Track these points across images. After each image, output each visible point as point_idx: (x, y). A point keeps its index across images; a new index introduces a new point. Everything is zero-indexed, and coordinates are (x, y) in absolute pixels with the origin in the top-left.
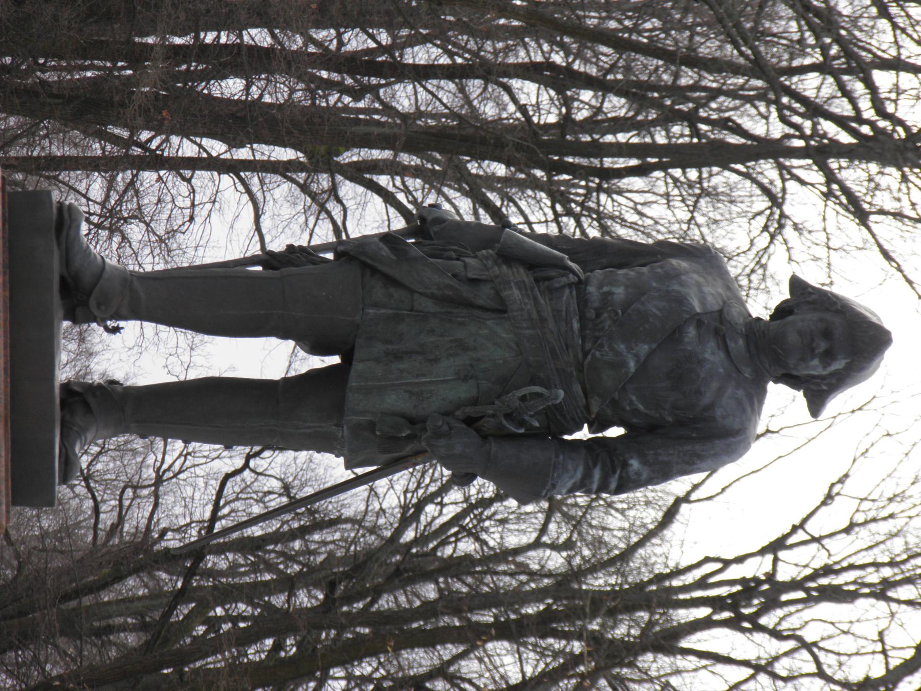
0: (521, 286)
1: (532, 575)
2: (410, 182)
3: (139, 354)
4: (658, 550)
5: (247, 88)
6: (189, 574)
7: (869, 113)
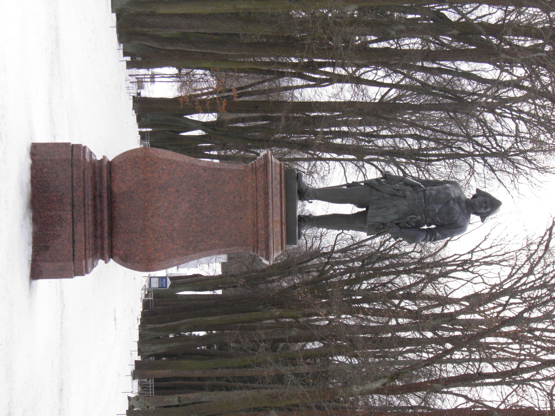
0: (410, 191)
1: (413, 259)
2: (382, 163)
3: (318, 208)
4: (443, 253)
5: (342, 141)
6: (329, 258)
7: (495, 146)
